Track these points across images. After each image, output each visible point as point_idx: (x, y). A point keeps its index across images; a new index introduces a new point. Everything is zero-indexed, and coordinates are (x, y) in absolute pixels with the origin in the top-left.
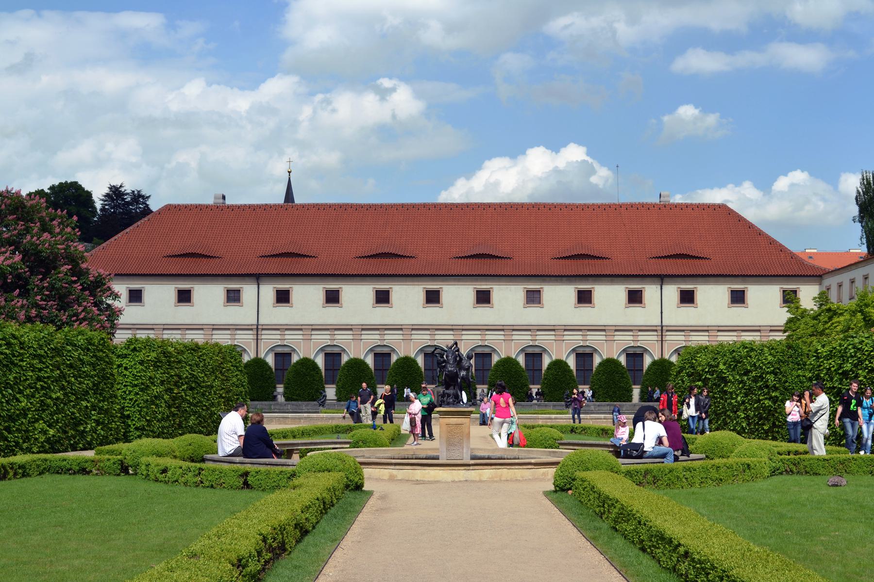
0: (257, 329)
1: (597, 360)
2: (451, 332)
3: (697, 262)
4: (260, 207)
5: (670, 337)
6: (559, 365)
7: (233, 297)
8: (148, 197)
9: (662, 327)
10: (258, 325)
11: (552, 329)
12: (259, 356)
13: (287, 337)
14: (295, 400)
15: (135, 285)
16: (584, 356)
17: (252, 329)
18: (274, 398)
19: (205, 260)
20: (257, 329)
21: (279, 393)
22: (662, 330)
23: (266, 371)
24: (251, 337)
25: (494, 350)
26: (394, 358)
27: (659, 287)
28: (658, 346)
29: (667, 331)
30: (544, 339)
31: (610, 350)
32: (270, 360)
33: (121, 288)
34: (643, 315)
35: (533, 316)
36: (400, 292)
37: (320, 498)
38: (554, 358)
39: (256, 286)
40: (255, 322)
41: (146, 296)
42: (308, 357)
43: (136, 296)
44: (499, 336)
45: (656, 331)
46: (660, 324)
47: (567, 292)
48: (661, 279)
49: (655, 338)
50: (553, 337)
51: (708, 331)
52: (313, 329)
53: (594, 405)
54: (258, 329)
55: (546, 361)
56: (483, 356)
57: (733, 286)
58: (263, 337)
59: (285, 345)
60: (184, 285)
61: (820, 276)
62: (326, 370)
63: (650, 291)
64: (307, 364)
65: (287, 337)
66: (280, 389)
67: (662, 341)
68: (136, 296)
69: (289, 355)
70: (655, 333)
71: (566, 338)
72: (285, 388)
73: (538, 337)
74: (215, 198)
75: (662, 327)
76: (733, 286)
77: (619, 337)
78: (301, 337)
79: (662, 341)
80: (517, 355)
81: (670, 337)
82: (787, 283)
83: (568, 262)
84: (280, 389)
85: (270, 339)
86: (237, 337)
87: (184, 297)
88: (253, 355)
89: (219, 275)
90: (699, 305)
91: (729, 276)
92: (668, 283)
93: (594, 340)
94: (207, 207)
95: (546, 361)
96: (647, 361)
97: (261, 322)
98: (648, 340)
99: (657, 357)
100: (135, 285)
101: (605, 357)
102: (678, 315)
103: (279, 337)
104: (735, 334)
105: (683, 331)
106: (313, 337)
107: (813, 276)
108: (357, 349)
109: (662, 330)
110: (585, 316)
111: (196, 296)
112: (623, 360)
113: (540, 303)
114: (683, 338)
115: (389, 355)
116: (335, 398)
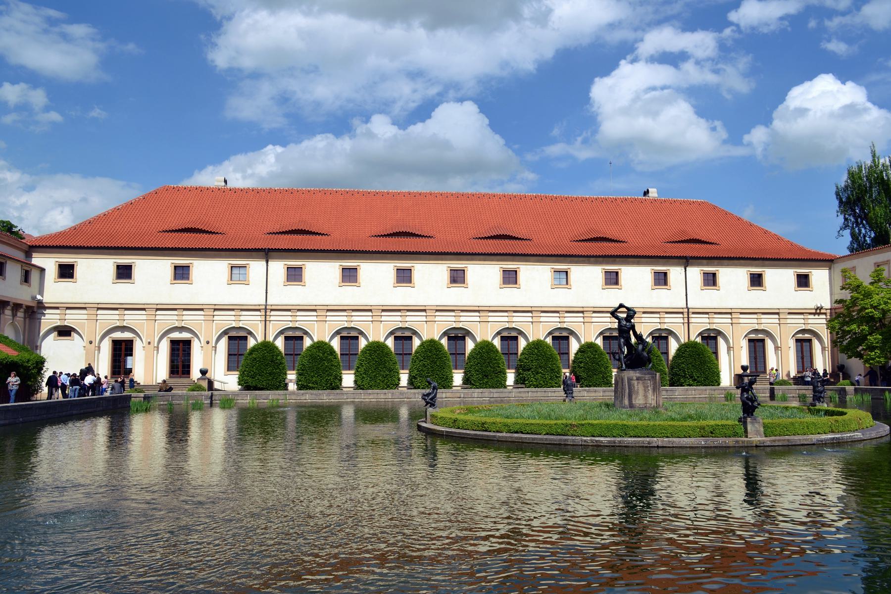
0: (266, 309)
1: (363, 343)
2: (477, 314)
5: (274, 316)
6: (322, 347)
7: (661, 279)
8: (837, 188)
9: (266, 305)
10: (266, 305)
13: (298, 318)
14: (311, 388)
15: (66, 259)
16: (349, 337)
18: (285, 387)
19: (206, 236)
20: (266, 309)
21: (291, 381)
22: (687, 313)
23: (277, 356)
24: (259, 318)
26: (307, 342)
28: (261, 326)
29: (272, 310)
33: (49, 263)
36: (201, 267)
39: (264, 263)
41: (136, 272)
43: (66, 272)
45: (682, 313)
47: (385, 270)
48: (686, 261)
49: (681, 320)
51: (730, 313)
54: (266, 310)
56: (403, 337)
58: (272, 318)
60: (124, 260)
63: (675, 273)
66: (292, 376)
67: (688, 323)
68: (66, 272)
70: (681, 316)
72: (299, 374)
77: (387, 317)
78: (315, 318)
79: (688, 323)
80: (441, 338)
82: (708, 265)
83: (588, 244)
84: (292, 376)
85: (280, 322)
86: (242, 318)
89: (222, 250)
90: (362, 285)
92: (693, 265)
93: (413, 321)
98: (674, 323)
100: (66, 259)
101: (316, 340)
102: (702, 298)
103: (290, 318)
104: (755, 316)
106: (328, 318)
108: (321, 331)
110: (124, 293)
112: (390, 343)
114: (707, 320)
116: (353, 385)
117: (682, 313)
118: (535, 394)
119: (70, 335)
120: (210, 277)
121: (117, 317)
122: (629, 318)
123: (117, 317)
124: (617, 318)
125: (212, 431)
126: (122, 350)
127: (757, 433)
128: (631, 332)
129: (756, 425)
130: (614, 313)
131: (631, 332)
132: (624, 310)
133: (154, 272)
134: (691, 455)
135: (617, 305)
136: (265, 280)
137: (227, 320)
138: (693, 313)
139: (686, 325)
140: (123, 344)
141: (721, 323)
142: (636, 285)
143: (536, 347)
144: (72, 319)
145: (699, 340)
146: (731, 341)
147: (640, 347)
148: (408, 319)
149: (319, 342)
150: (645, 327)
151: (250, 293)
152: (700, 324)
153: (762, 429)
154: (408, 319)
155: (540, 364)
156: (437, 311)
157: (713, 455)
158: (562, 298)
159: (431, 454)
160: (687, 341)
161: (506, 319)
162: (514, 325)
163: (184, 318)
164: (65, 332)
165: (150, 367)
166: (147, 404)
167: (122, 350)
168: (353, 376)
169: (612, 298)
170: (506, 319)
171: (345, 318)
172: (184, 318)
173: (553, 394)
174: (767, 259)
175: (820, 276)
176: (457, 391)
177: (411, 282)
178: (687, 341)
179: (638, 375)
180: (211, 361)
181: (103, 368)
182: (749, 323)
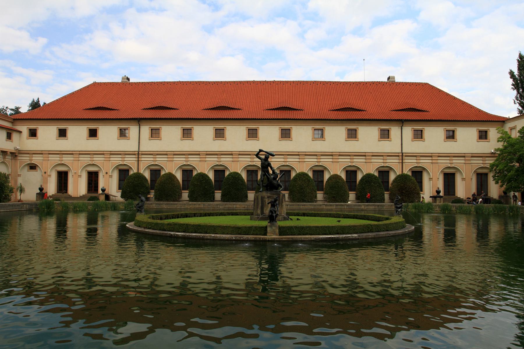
0: (138, 154)
3: (421, 113)
4: (148, 83)
7: (122, 134)
10: (139, 152)
11: (331, 155)
12: (140, 172)
17: (135, 154)
20: (138, 154)
22: (402, 156)
24: (397, 161)
25: (293, 168)
27: (400, 128)
30: (325, 161)
31: (368, 168)
32: (147, 175)
34: (391, 146)
35: (187, 146)
36: (104, 130)
37: (413, 276)
38: (365, 174)
40: (137, 150)
42: (336, 173)
44: (295, 159)
45: (398, 156)
46: (400, 151)
48: (402, 122)
49: (397, 161)
50: (463, 162)
51: (431, 156)
52: (174, 154)
53: (364, 205)
55: (326, 176)
56: (286, 172)
57: (447, 128)
58: (406, 161)
59: (156, 165)
60: (93, 127)
61: (504, 122)
62: (215, 181)
63: (395, 131)
64: (236, 176)
65: (158, 159)
69: (191, 171)
70: (398, 158)
71: (207, 159)
73: (322, 160)
74: (123, 78)
75: (402, 154)
76: (447, 128)
77: (342, 160)
78: (166, 159)
79: (402, 163)
81: (143, 158)
87: (93, 133)
88: (135, 171)
90: (195, 138)
91: (463, 121)
93: (358, 162)
94: (117, 83)
95: (326, 176)
96: (392, 177)
97: (141, 149)
98: (393, 163)
99: (399, 173)
102: (412, 146)
103: (152, 159)
105: (416, 156)
107: (497, 121)
108: (205, 168)
109: (402, 155)
110: (93, 145)
111: (100, 133)
113: (486, 138)
115: (224, 171)
116: (188, 199)
117: (398, 156)
118: (292, 207)
119: (35, 169)
120: (108, 136)
121: (58, 159)
122: (267, 158)
123: (58, 159)
124: (260, 158)
125: (109, 227)
126: (63, 178)
127: (275, 234)
128: (269, 168)
129: (274, 228)
130: (257, 155)
131: (269, 168)
132: (264, 153)
133: (78, 134)
134: (323, 247)
135: (258, 151)
136: (139, 138)
137: (117, 160)
138: (406, 156)
139: (401, 164)
140: (94, 174)
141: (424, 163)
142: (269, 138)
143: (368, 177)
144: (36, 160)
145: (410, 174)
146: (431, 174)
147: (272, 176)
148: (222, 159)
149: (367, 174)
150: (276, 163)
151: (129, 145)
152: (410, 164)
153: (278, 231)
154: (222, 159)
155: (199, 186)
156: (239, 154)
157: (329, 247)
158: (319, 146)
159: (139, 244)
160: (401, 173)
161: (283, 160)
162: (354, 164)
163: (94, 159)
164: (33, 167)
165: (78, 187)
166: (77, 210)
167: (63, 178)
168: (355, 195)
169: (254, 146)
170: (283, 160)
171: (184, 159)
172: (94, 159)
173: (303, 207)
174: (457, 121)
175: (493, 133)
176: (321, 203)
177: (388, 138)
178: (401, 173)
179: (269, 195)
180: (110, 184)
181: (51, 189)
182: (444, 163)
